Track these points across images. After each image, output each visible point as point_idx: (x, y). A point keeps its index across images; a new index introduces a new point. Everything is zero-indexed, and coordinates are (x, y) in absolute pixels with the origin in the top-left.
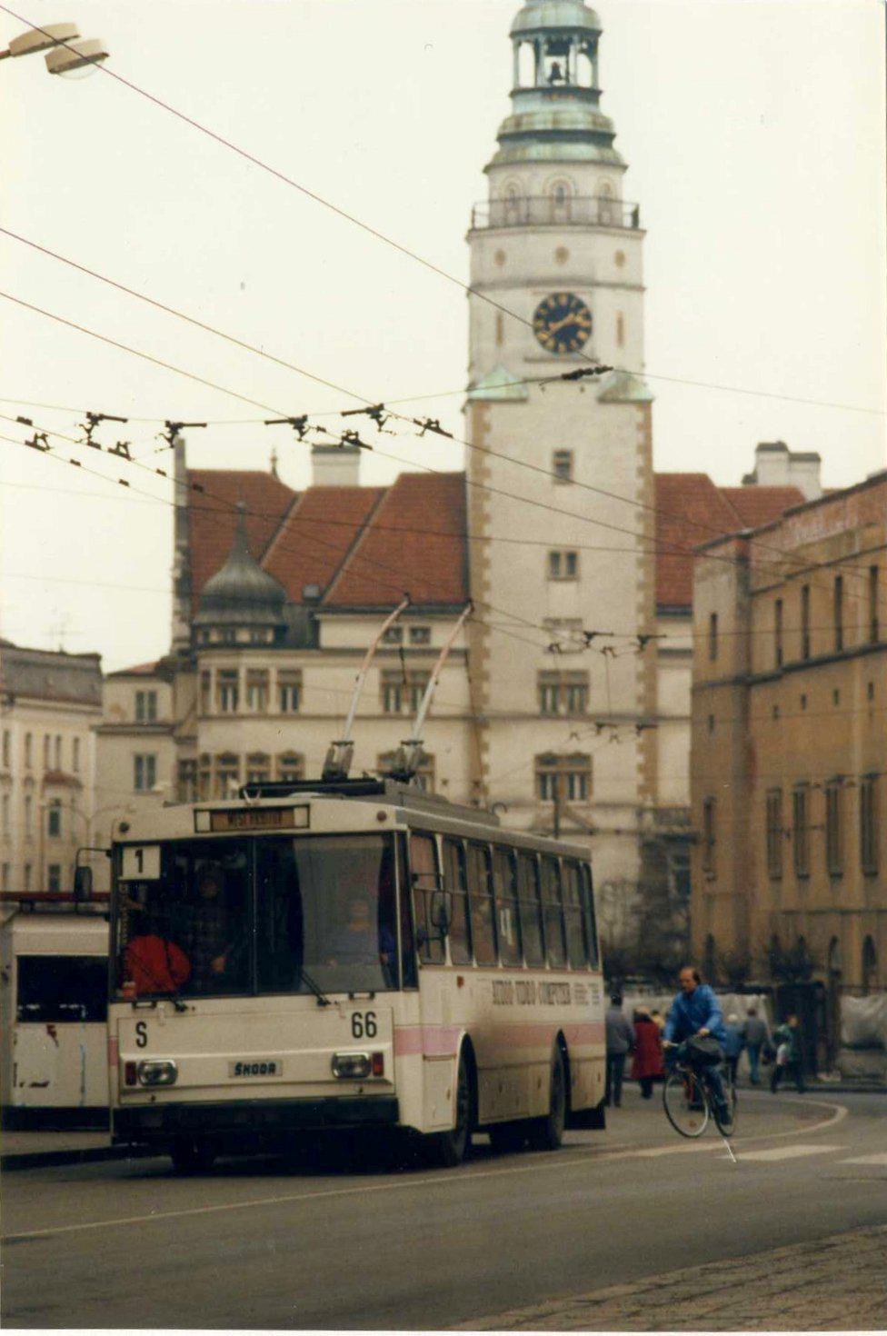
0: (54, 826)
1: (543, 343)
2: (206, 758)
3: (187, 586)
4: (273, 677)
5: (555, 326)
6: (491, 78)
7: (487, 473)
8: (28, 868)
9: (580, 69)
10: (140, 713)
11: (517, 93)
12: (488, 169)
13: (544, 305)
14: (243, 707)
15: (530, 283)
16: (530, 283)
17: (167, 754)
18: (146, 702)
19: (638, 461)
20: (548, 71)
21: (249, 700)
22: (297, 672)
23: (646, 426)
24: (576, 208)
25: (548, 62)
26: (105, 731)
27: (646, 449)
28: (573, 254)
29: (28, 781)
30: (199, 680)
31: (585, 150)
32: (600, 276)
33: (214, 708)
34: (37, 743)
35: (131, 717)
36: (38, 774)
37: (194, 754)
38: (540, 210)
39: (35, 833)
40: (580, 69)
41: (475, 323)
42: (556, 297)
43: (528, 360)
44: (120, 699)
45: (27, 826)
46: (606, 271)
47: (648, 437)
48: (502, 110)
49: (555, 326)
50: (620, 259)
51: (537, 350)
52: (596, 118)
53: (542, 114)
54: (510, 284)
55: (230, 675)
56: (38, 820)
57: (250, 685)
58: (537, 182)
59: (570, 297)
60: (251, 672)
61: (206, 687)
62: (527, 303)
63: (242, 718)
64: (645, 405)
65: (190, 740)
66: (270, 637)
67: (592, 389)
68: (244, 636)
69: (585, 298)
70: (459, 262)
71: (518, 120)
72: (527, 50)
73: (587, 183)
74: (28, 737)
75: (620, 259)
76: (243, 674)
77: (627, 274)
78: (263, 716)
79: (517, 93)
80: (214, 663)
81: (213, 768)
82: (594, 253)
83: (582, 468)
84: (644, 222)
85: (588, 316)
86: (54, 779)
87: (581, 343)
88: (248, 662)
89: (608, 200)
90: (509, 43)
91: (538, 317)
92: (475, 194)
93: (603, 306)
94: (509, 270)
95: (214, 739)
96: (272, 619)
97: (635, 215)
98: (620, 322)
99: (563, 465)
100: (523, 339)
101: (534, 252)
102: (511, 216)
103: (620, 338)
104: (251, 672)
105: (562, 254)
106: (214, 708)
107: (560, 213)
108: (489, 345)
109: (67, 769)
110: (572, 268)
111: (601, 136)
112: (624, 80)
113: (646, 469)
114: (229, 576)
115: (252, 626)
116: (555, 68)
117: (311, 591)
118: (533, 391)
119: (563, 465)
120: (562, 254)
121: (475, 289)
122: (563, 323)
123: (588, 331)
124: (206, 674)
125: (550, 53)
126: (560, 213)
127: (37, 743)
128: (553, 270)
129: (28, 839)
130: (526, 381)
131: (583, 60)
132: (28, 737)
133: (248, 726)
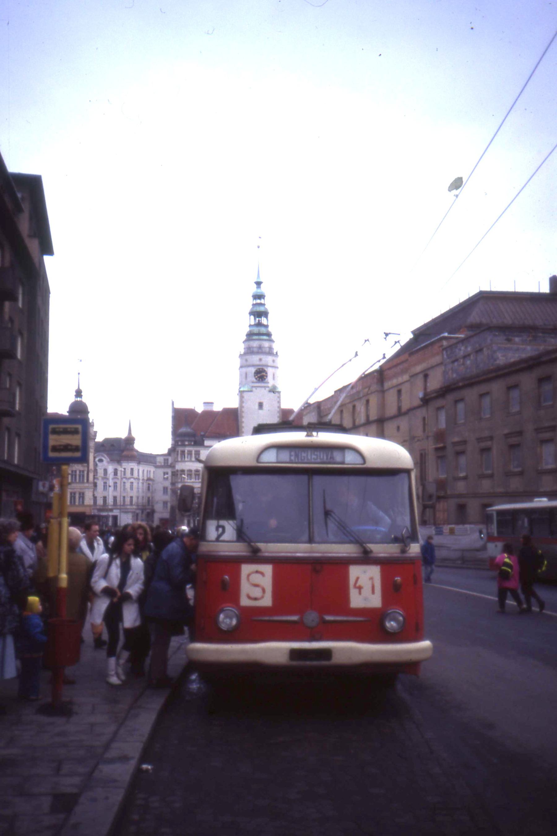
0: (149, 489)
1: (256, 379)
2: (177, 471)
3: (175, 433)
4: (193, 452)
5: (259, 375)
6: (246, 322)
7: (243, 407)
8: (143, 497)
9: (264, 321)
10: (165, 463)
11: (250, 326)
12: (243, 342)
13: (256, 371)
14: (186, 459)
15: (253, 366)
16: (253, 366)
17: (169, 471)
18: (166, 461)
19: (276, 405)
20: (257, 321)
21: (188, 458)
22: (199, 451)
23: (279, 397)
24: (264, 350)
25: (257, 319)
26: (157, 467)
27: (279, 402)
28: (263, 359)
29: (143, 480)
30: (176, 453)
31: (265, 337)
32: (269, 365)
33: (179, 459)
34: (145, 472)
35: (163, 464)
36: (145, 478)
37: (175, 470)
38: (255, 350)
39: (145, 490)
40: (264, 321)
41: (241, 375)
42: (259, 369)
43: (253, 382)
44: (160, 460)
45: (143, 489)
46: (270, 363)
47: (280, 400)
48: (247, 329)
49: (259, 375)
50: (274, 361)
51: (255, 380)
52: (268, 331)
53: (256, 330)
54: (249, 366)
55: (183, 452)
56: (146, 485)
57: (188, 454)
58: (255, 344)
59: (262, 369)
60: (188, 451)
61: (178, 454)
62: (253, 370)
63: (186, 461)
64: (279, 392)
65: (174, 467)
66: (193, 443)
67: (267, 389)
68: (187, 443)
69: (266, 369)
70: (238, 362)
71: (250, 331)
72: (252, 317)
73: (266, 344)
74: (143, 471)
75: (274, 361)
76: (186, 451)
77: (275, 365)
78: (191, 461)
79: (250, 326)
80: (180, 449)
81: (179, 473)
82: (268, 360)
83: (265, 406)
84: (278, 354)
85: (266, 373)
86: (149, 479)
87: (265, 379)
88: (187, 449)
89: (271, 348)
90: (249, 315)
91: (255, 373)
92: (241, 349)
93: (270, 371)
94: (248, 363)
95: (179, 466)
96: (193, 439)
97: (277, 353)
98: (274, 375)
99: (261, 405)
100: (252, 378)
101: (255, 359)
102: (249, 351)
103: (274, 378)
104: (188, 451)
105: (260, 360)
106: (179, 459)
107: (260, 351)
108: (244, 380)
109: (152, 477)
110: (263, 362)
111: (269, 335)
112: (273, 323)
113: (279, 407)
114: (183, 430)
115: (188, 441)
116: (259, 320)
117: (202, 433)
118: (254, 389)
119: (261, 405)
120: (260, 360)
121: (241, 367)
122: (261, 375)
123: (267, 376)
124: (178, 452)
125: (258, 317)
126: (260, 351)
127: (145, 472)
128: (258, 363)
129: (143, 492)
130: (252, 387)
131: (265, 319)
132: (143, 471)
133: (187, 463)
